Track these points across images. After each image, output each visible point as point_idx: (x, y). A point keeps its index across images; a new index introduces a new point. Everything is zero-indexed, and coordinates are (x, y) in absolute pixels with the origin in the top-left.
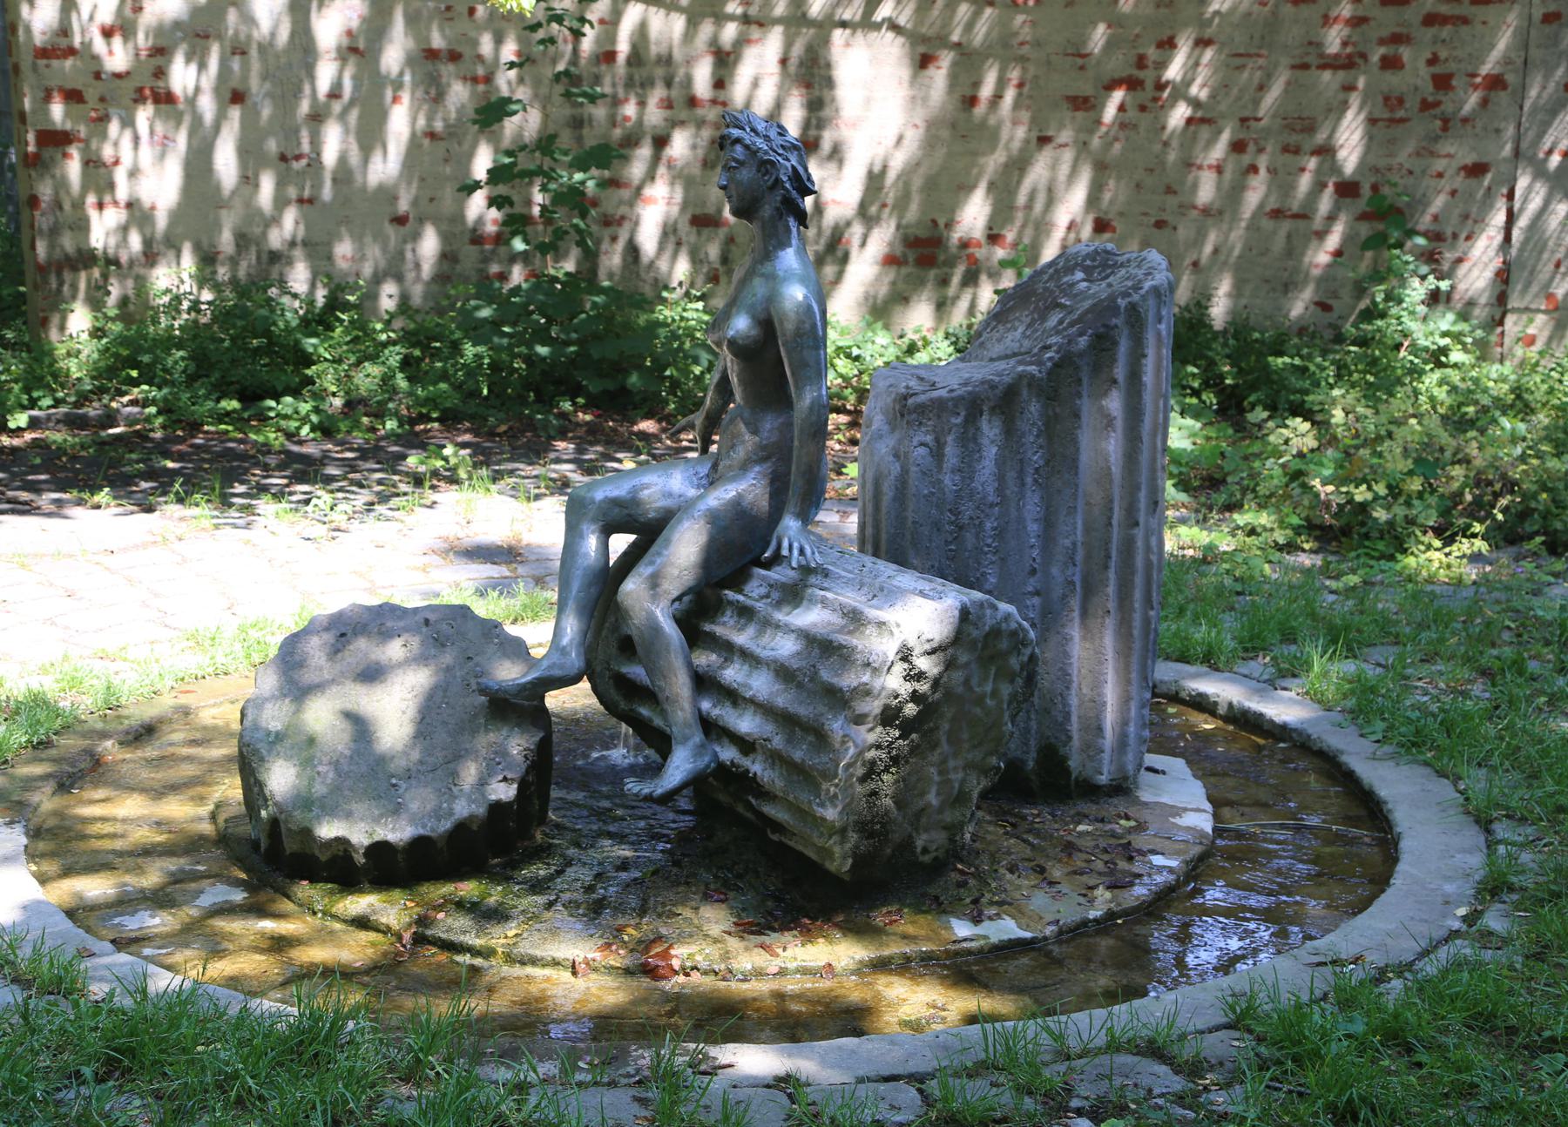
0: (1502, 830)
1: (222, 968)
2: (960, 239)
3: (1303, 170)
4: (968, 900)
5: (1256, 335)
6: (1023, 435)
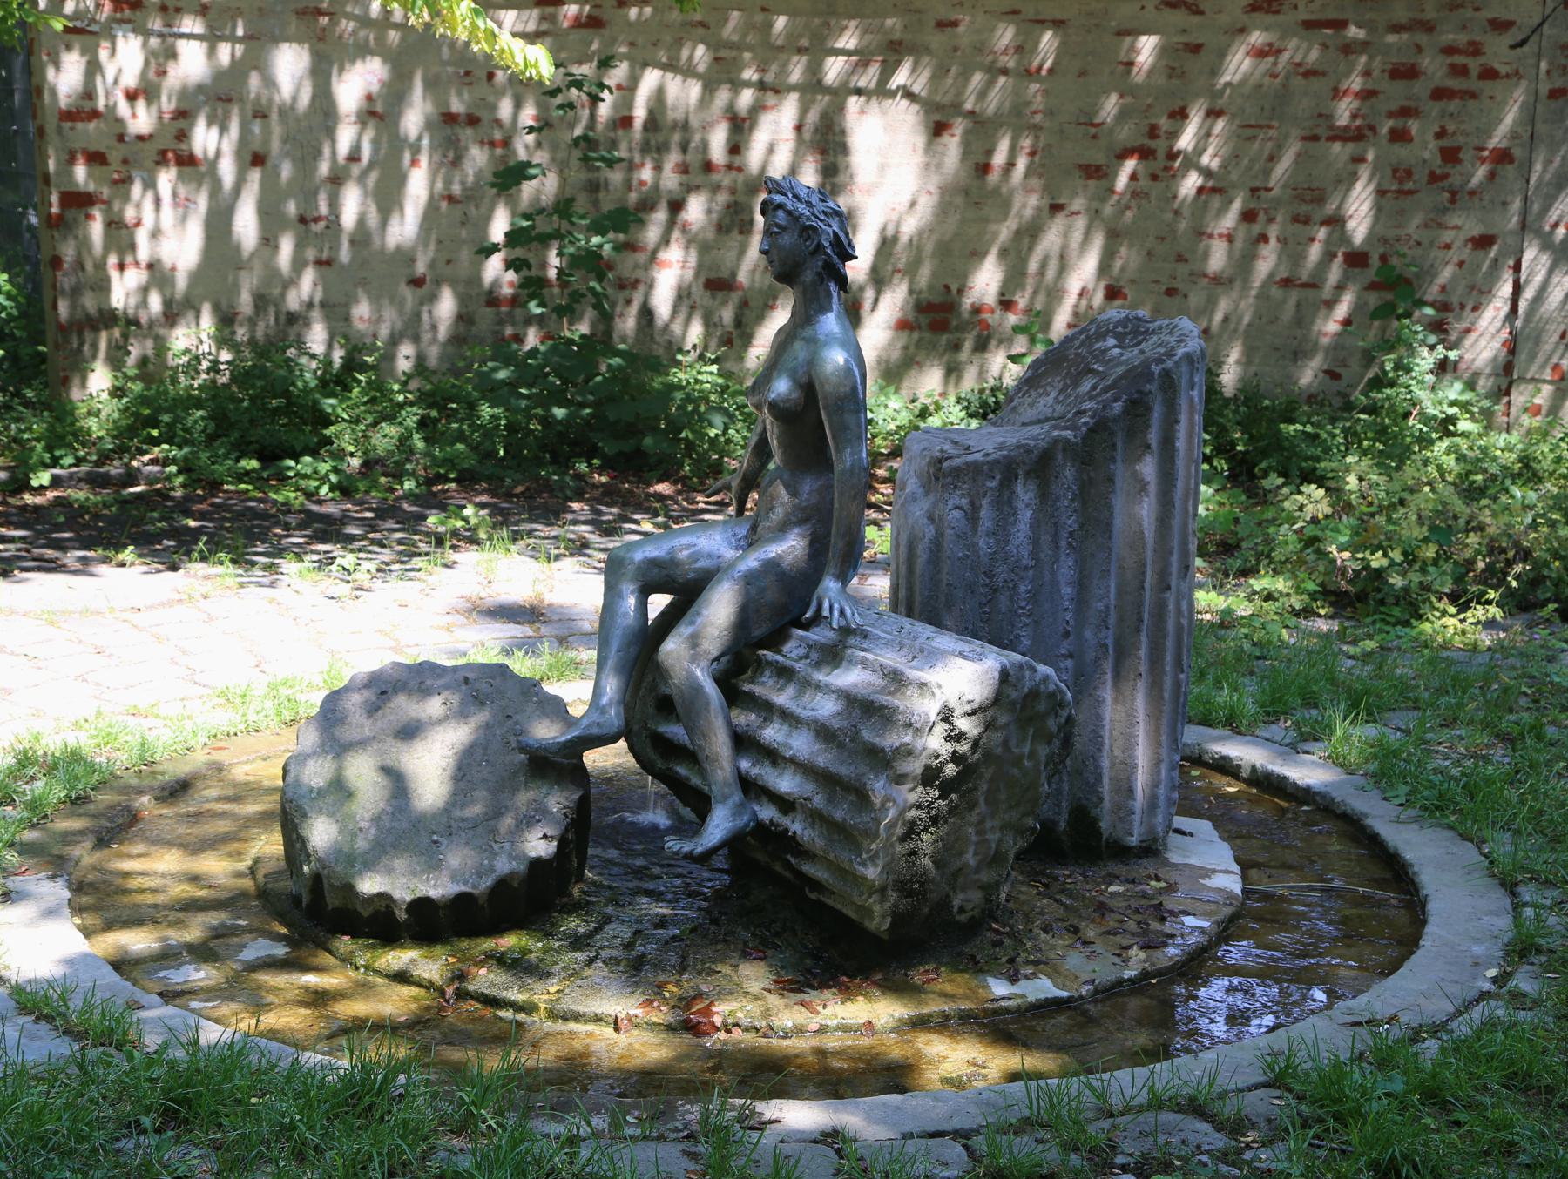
0: (1527, 893)
1: (270, 1020)
2: (973, 305)
3: (1312, 240)
4: (1004, 960)
5: (1267, 402)
6: (1058, 499)
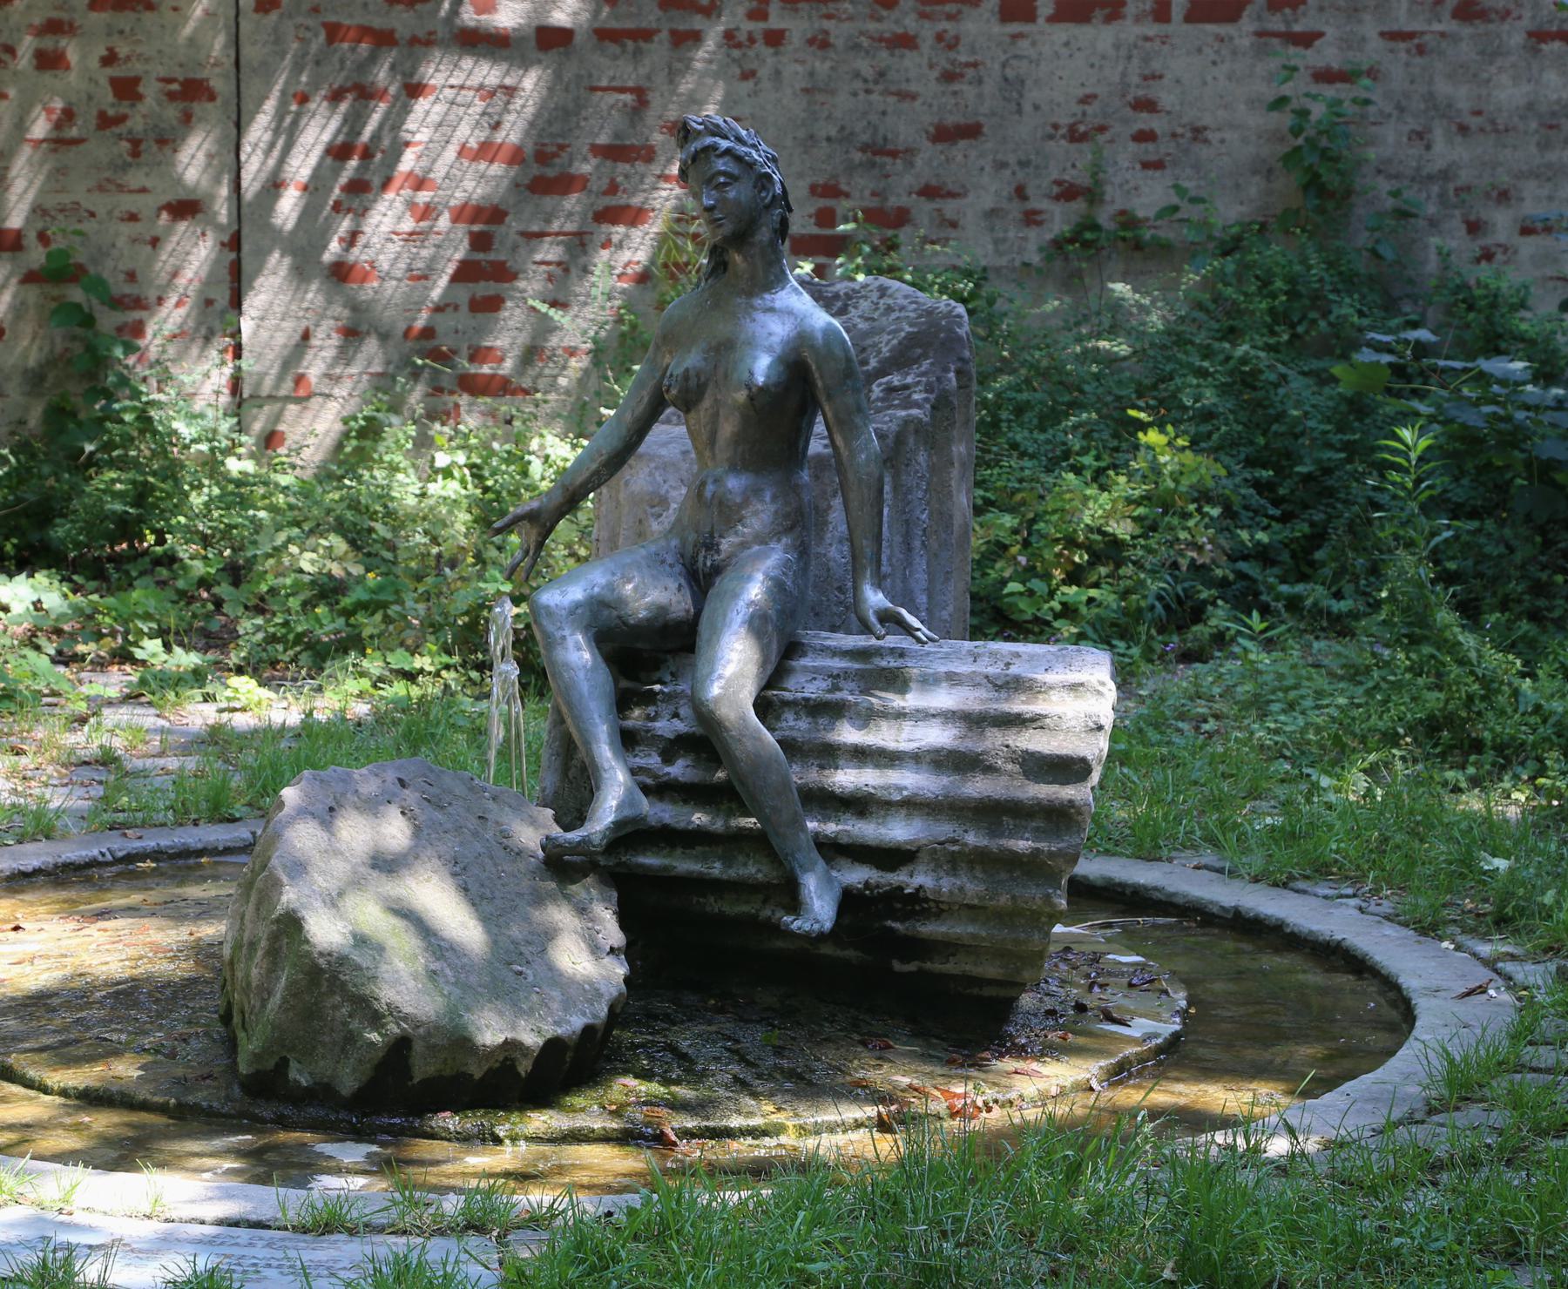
6: (909, 491)
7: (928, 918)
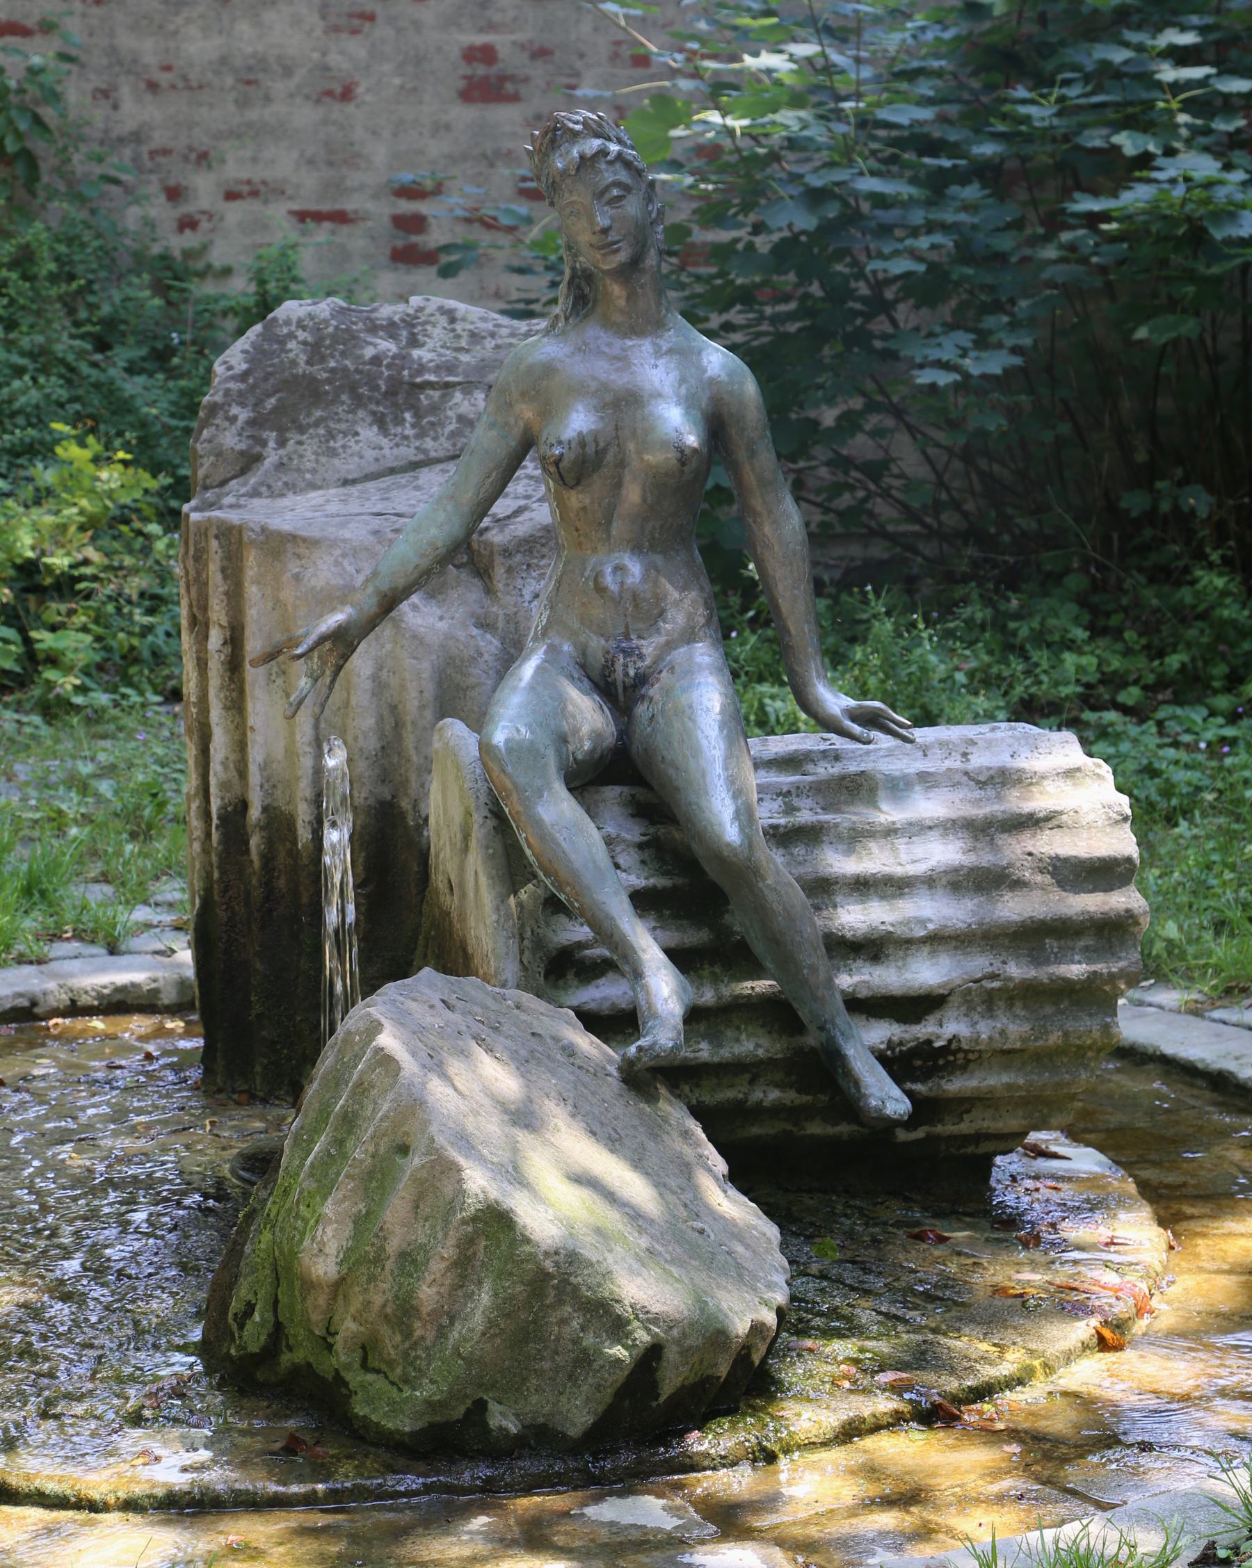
7: (952, 1073)
